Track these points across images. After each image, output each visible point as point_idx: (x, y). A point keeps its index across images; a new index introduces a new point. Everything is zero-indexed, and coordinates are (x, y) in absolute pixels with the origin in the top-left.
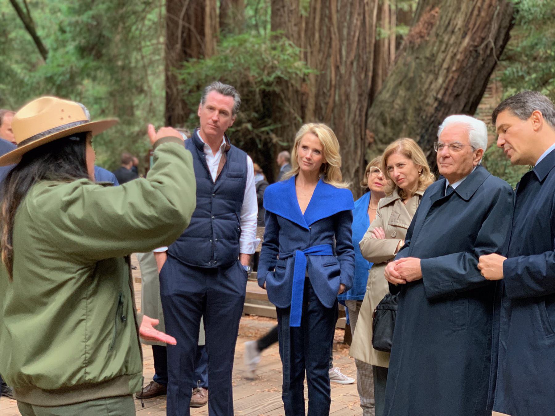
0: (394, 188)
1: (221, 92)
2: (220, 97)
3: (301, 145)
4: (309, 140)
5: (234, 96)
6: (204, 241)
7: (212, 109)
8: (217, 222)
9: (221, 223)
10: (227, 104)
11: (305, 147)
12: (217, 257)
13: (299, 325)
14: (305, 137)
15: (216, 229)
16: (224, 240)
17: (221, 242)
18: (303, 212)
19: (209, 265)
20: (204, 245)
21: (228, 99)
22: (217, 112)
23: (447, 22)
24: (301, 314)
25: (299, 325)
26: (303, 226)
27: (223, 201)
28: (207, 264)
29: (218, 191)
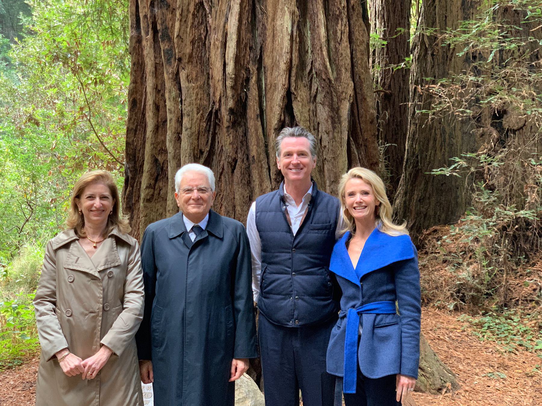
0: (123, 309)
1: (293, 135)
2: (293, 140)
3: (346, 195)
4: (353, 185)
5: (306, 136)
6: (284, 299)
7: (289, 154)
8: (299, 278)
9: (302, 280)
10: (302, 144)
11: (352, 194)
12: (298, 315)
13: (354, 392)
14: (347, 185)
15: (296, 286)
16: (306, 298)
17: (302, 299)
18: (355, 267)
19: (291, 324)
20: (284, 303)
21: (303, 139)
22: (295, 156)
23: (315, 91)
24: (355, 379)
25: (354, 392)
26: (353, 281)
27: (304, 256)
28: (289, 323)
29: (300, 245)
